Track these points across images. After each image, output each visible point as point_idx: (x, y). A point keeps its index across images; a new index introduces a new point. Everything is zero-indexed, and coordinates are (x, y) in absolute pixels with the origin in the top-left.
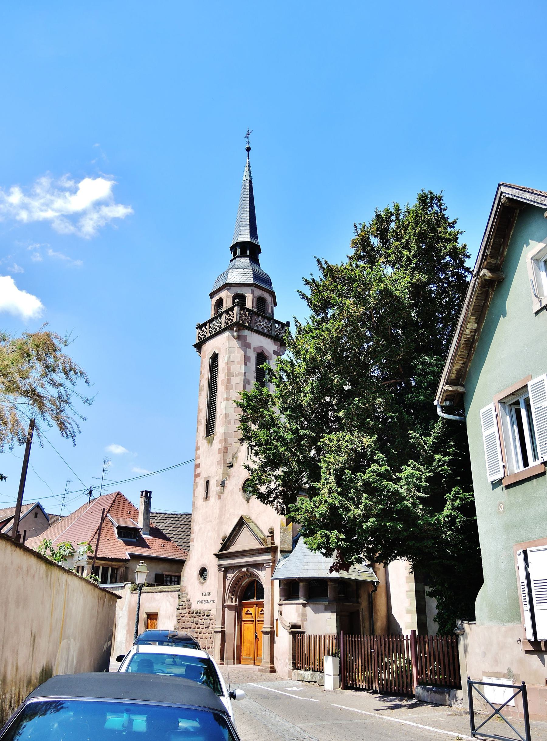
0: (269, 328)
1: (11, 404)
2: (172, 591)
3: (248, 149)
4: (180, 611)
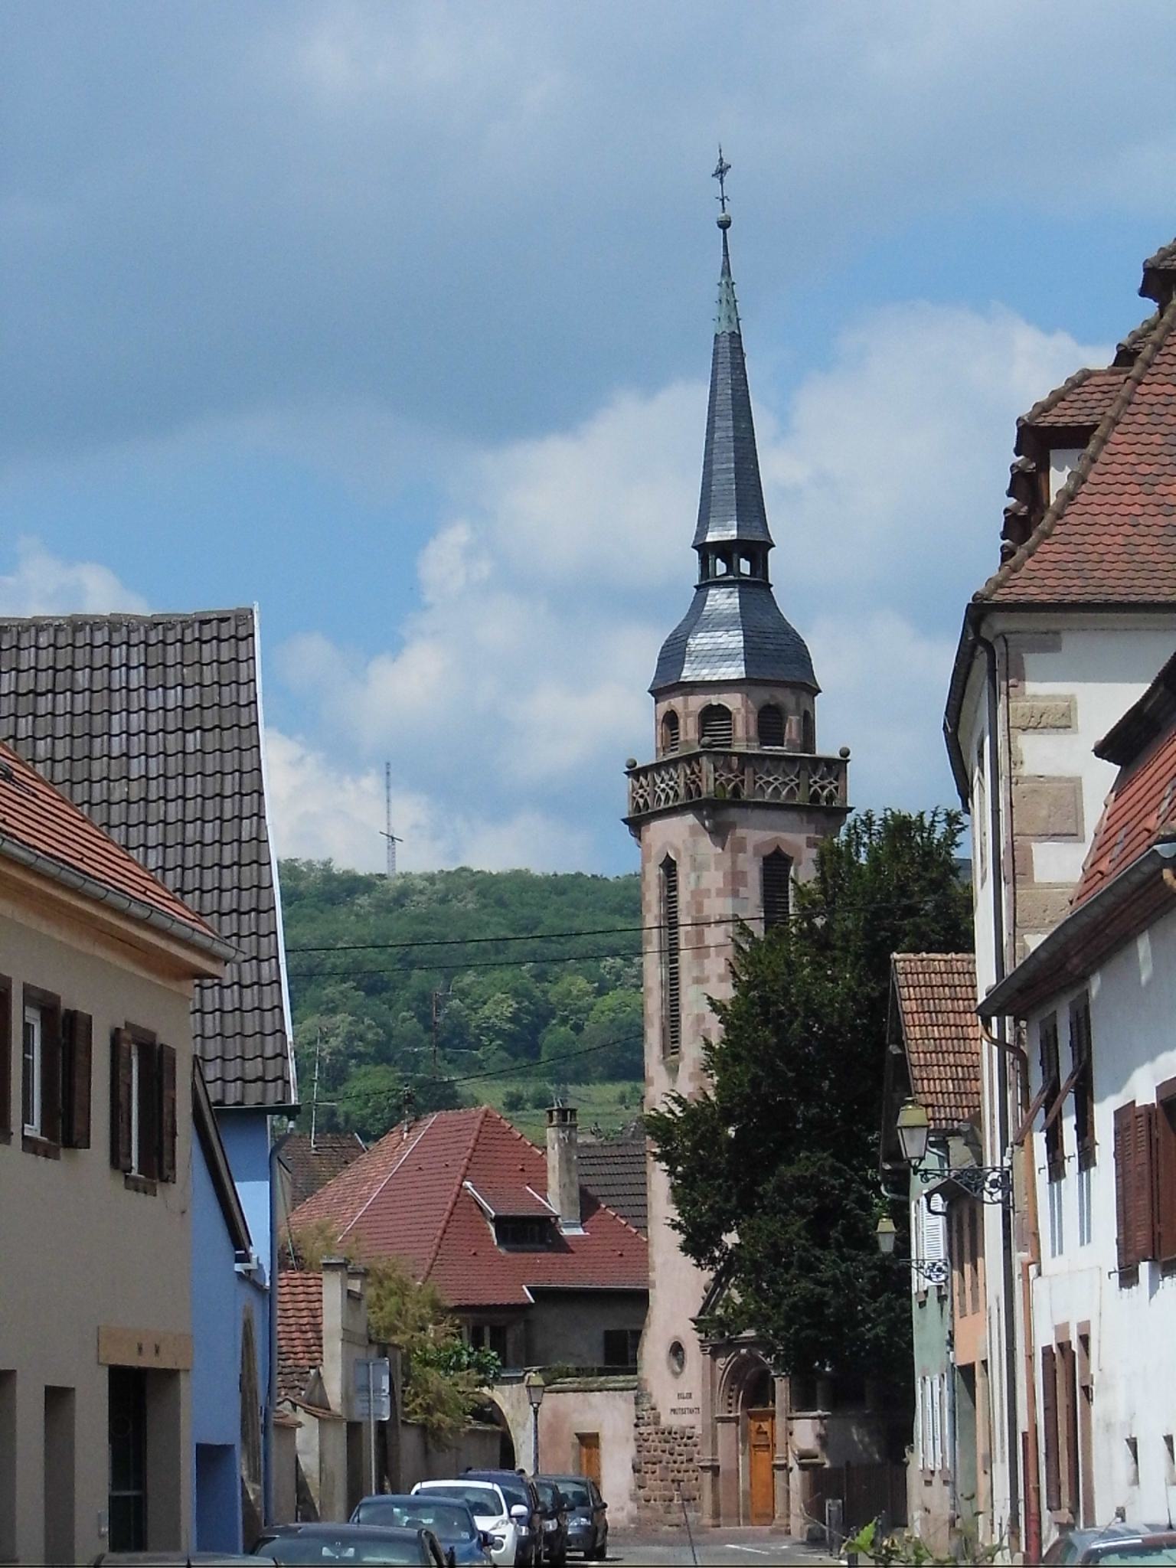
0: (793, 784)
1: (471, 1403)
2: (622, 1389)
3: (724, 225)
4: (642, 1429)
